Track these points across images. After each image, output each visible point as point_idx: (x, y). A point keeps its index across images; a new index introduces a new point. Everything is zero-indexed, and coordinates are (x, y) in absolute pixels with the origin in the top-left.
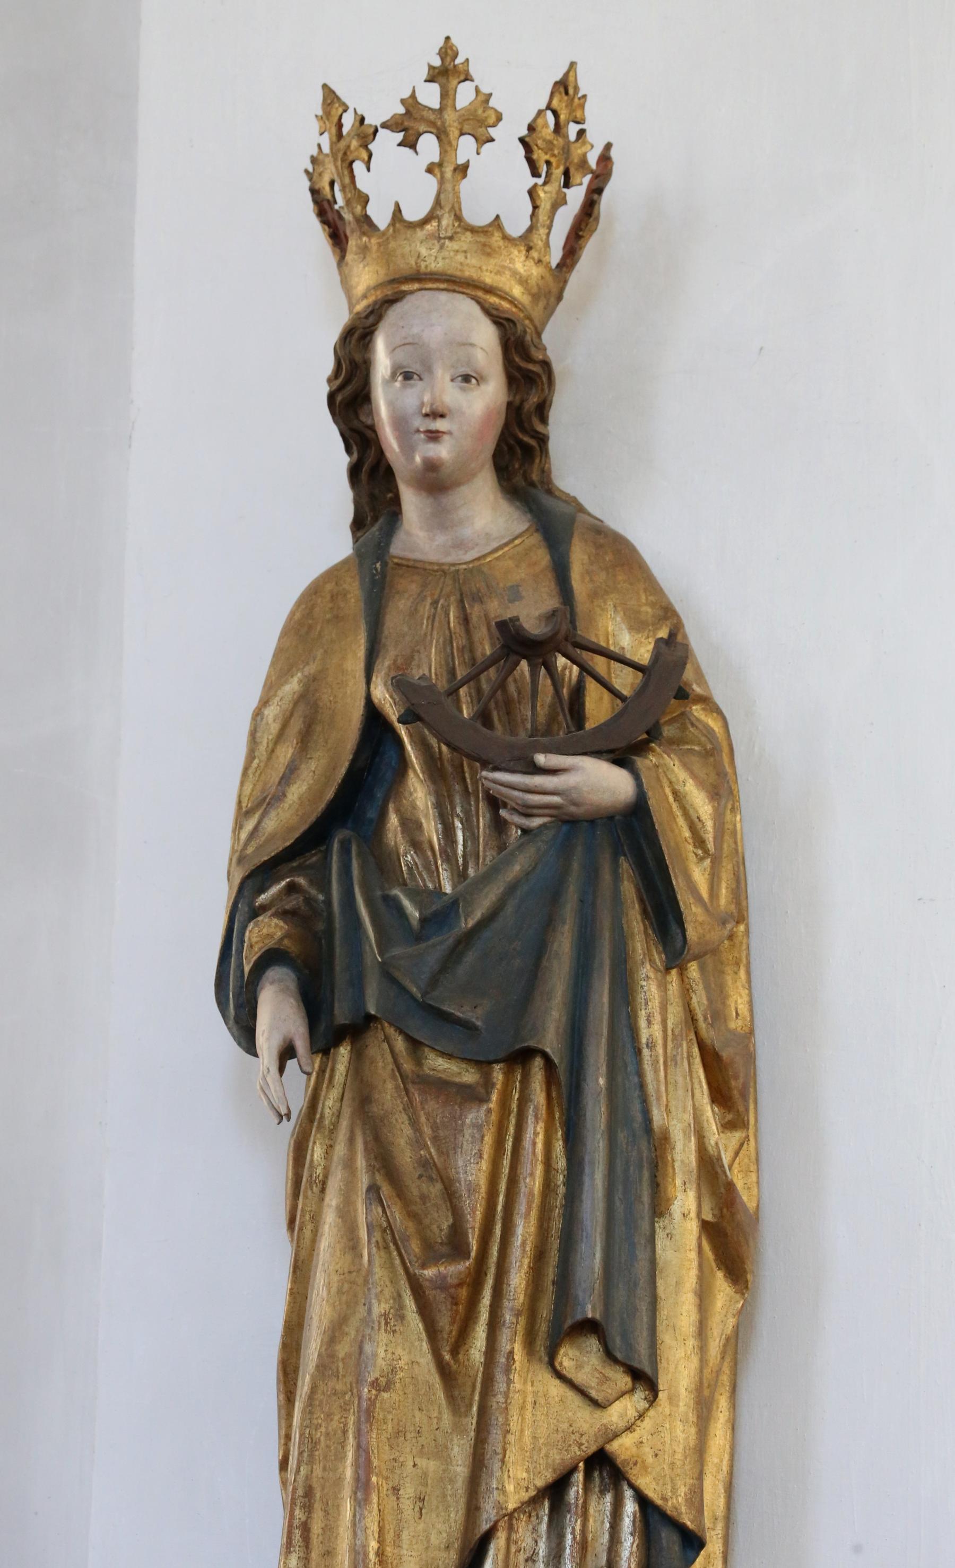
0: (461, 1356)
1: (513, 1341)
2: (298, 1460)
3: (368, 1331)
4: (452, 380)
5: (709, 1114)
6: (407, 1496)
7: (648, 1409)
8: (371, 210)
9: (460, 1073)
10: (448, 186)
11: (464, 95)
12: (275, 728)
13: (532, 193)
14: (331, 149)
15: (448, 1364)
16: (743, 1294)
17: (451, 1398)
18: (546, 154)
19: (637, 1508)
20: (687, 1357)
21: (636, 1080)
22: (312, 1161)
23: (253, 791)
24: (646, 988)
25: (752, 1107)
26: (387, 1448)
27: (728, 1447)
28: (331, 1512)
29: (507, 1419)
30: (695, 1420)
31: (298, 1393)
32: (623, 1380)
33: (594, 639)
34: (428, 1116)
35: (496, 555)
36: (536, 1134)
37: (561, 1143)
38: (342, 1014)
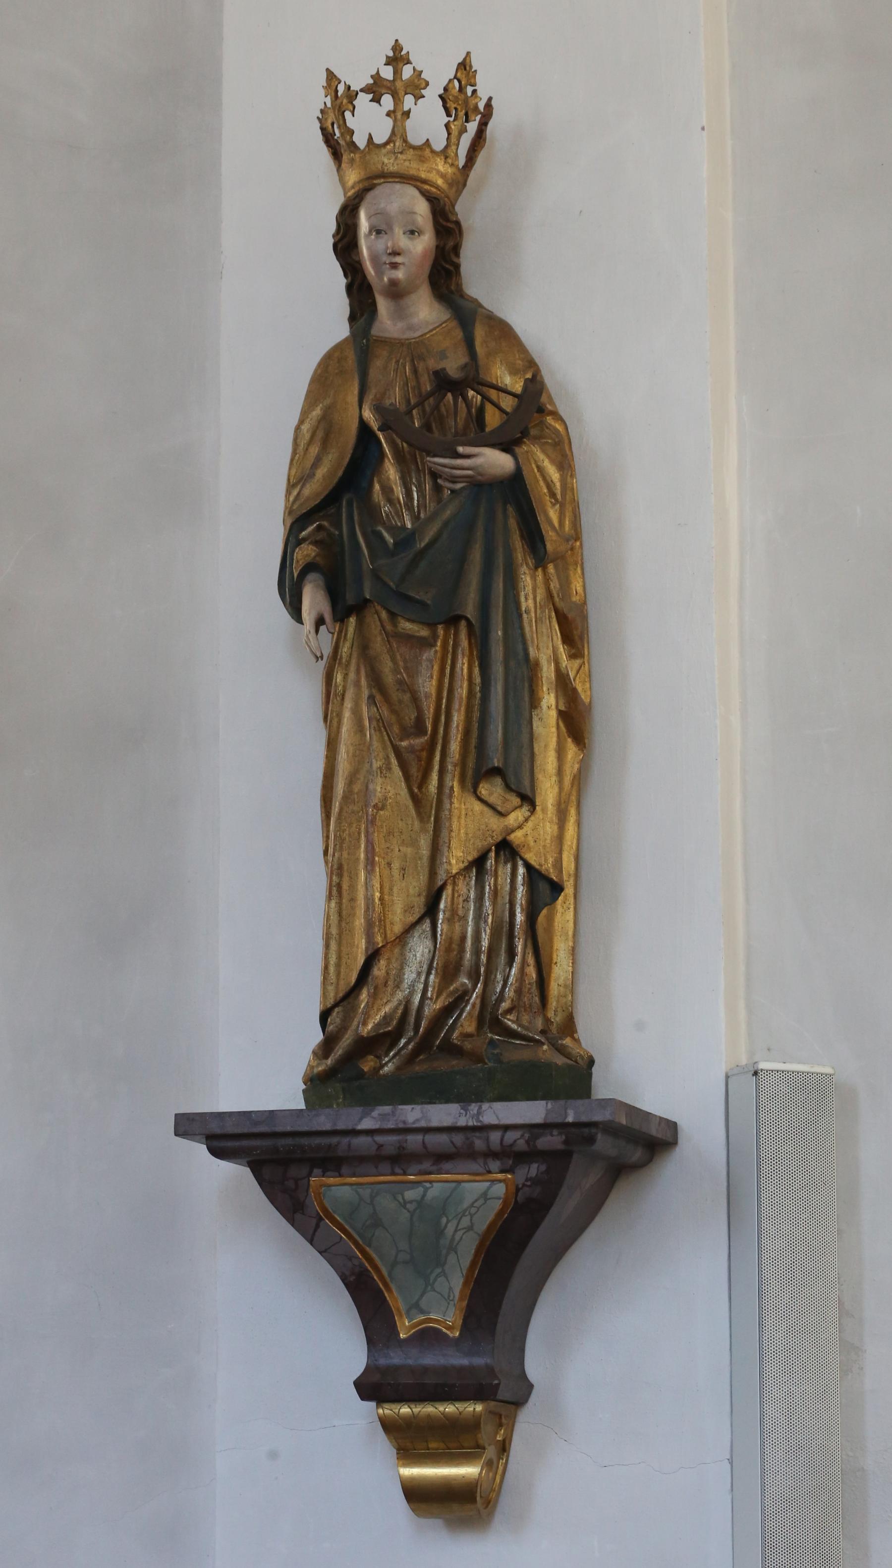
0: (423, 790)
1: (453, 780)
2: (334, 849)
3: (371, 777)
4: (404, 234)
5: (562, 649)
6: (395, 868)
7: (530, 816)
8: (355, 138)
9: (419, 631)
10: (399, 123)
11: (407, 72)
12: (307, 436)
13: (447, 126)
14: (332, 105)
15: (416, 794)
16: (583, 751)
17: (419, 813)
18: (454, 104)
19: (525, 871)
20: (552, 787)
21: (520, 631)
22: (336, 682)
23: (296, 473)
24: (524, 579)
25: (586, 646)
26: (383, 841)
27: (576, 836)
28: (354, 877)
29: (451, 824)
30: (557, 821)
31: (333, 811)
32: (516, 801)
33: (489, 380)
34: (401, 655)
35: (432, 333)
36: (463, 664)
37: (477, 668)
38: (350, 598)
